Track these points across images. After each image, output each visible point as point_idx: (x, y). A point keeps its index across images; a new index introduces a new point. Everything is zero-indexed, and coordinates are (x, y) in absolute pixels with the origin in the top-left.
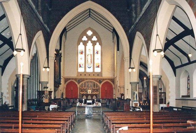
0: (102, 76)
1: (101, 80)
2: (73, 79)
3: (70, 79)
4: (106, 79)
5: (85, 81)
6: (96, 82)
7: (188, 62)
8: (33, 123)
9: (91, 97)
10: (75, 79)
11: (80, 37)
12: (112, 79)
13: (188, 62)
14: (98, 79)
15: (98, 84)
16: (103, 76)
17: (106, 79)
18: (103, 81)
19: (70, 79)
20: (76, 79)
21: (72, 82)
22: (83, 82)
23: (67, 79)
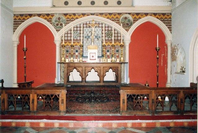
0: (132, 6)
1: (131, 18)
2: (39, 15)
3: (31, 15)
4: (146, 14)
5: (80, 19)
6: (114, 25)
7: (70, 80)
8: (191, 48)
9: (81, 75)
10: (48, 16)
11: (45, 7)
12: (164, 14)
13: (70, 80)
14: (119, 14)
15: (120, 28)
16: (136, 4)
17: (146, 14)
18: (135, 20)
19: (31, 15)
20: (48, 15)
21: (37, 25)
22: (72, 25)
23: (21, 15)
